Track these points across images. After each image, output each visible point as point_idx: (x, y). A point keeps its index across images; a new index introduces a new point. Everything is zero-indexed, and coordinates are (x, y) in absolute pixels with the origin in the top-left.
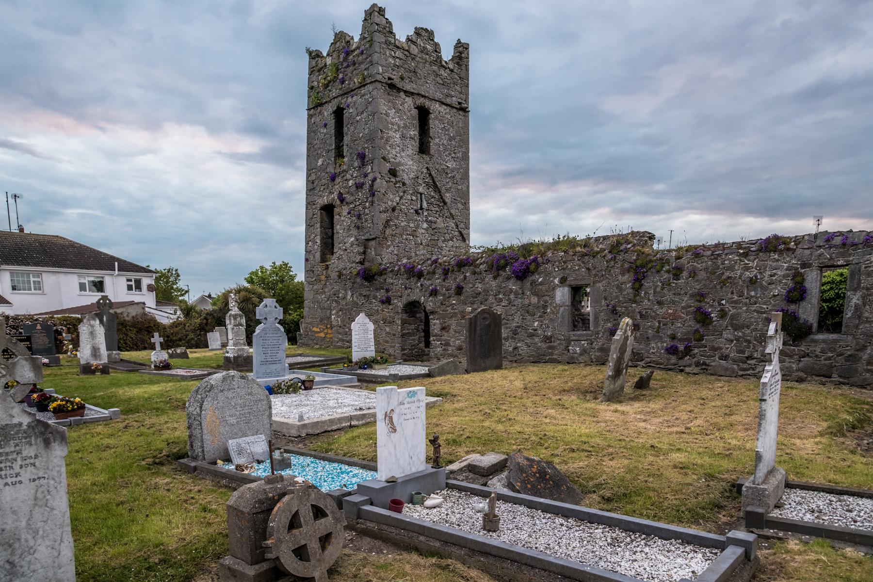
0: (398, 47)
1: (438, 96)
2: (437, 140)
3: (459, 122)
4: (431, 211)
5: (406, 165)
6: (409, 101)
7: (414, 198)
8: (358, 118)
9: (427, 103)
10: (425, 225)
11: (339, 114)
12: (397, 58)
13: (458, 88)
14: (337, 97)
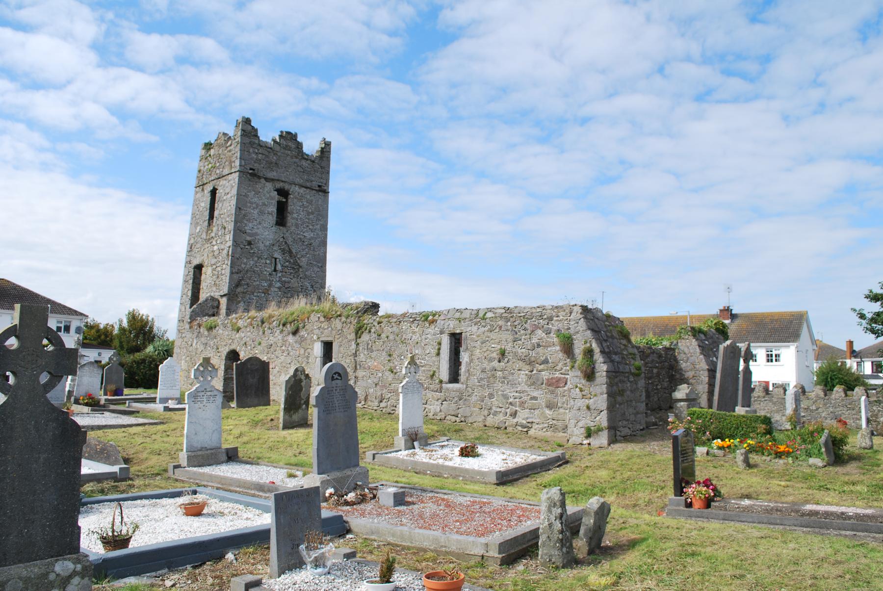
0: (261, 146)
1: (298, 180)
2: (295, 215)
3: (318, 201)
4: (286, 272)
5: (262, 235)
6: (269, 186)
7: (268, 262)
8: (225, 198)
9: (287, 187)
10: (278, 285)
11: (214, 192)
12: (260, 153)
13: (318, 174)
14: (213, 180)
